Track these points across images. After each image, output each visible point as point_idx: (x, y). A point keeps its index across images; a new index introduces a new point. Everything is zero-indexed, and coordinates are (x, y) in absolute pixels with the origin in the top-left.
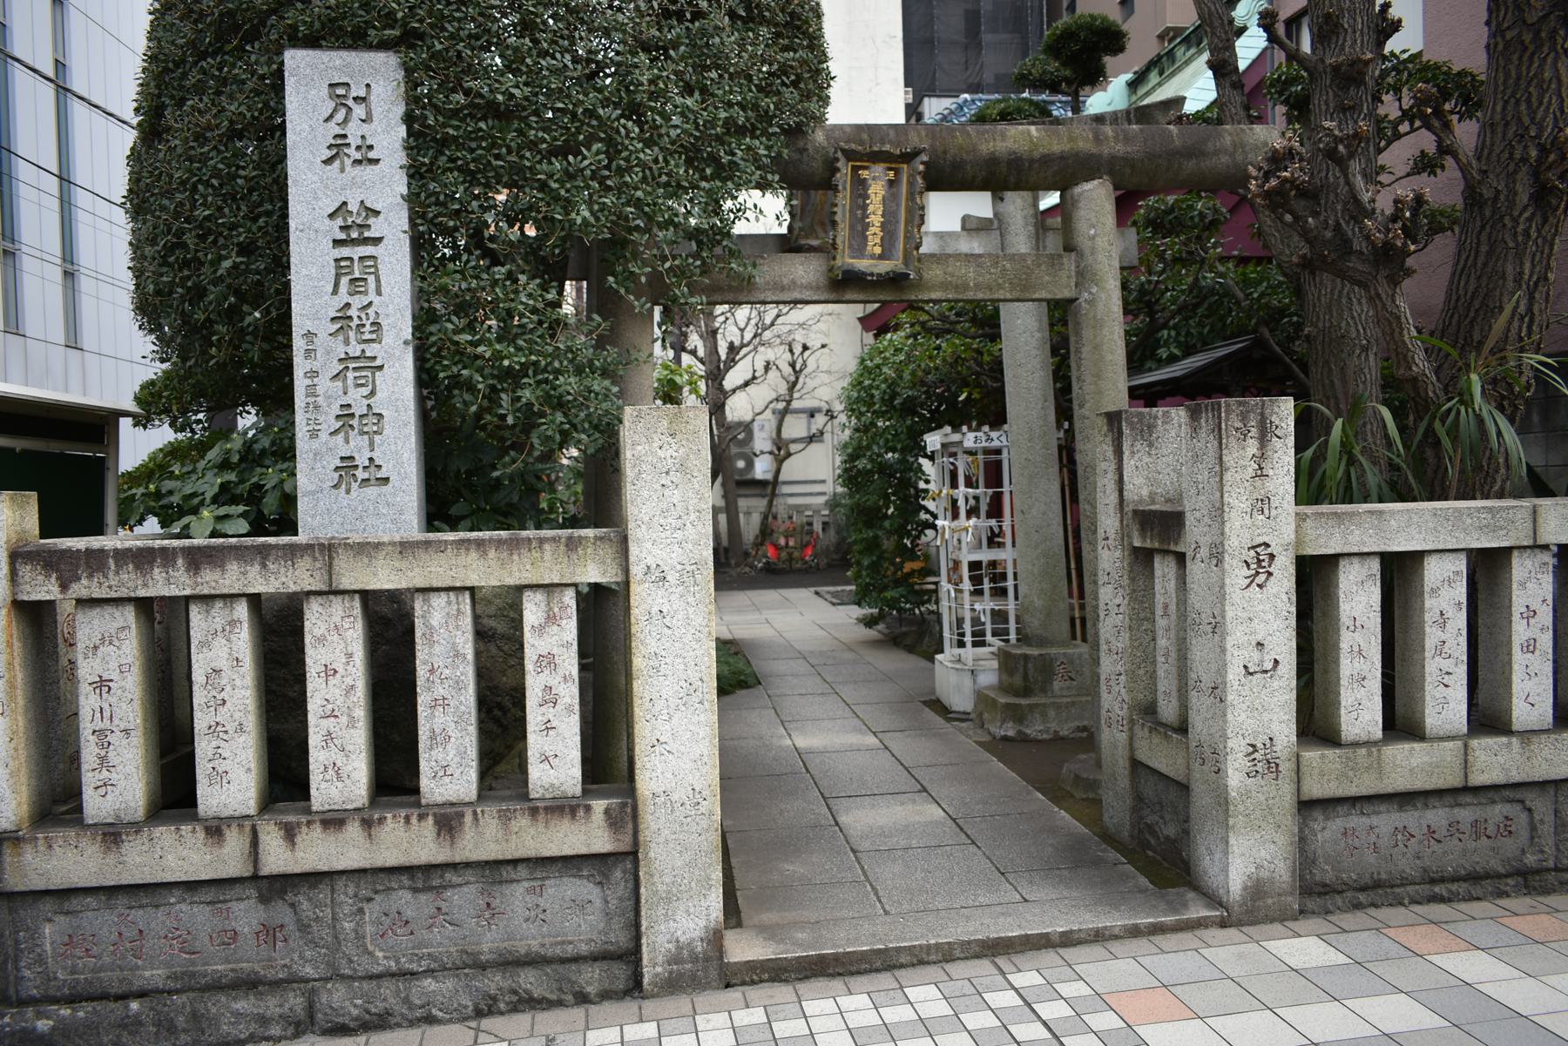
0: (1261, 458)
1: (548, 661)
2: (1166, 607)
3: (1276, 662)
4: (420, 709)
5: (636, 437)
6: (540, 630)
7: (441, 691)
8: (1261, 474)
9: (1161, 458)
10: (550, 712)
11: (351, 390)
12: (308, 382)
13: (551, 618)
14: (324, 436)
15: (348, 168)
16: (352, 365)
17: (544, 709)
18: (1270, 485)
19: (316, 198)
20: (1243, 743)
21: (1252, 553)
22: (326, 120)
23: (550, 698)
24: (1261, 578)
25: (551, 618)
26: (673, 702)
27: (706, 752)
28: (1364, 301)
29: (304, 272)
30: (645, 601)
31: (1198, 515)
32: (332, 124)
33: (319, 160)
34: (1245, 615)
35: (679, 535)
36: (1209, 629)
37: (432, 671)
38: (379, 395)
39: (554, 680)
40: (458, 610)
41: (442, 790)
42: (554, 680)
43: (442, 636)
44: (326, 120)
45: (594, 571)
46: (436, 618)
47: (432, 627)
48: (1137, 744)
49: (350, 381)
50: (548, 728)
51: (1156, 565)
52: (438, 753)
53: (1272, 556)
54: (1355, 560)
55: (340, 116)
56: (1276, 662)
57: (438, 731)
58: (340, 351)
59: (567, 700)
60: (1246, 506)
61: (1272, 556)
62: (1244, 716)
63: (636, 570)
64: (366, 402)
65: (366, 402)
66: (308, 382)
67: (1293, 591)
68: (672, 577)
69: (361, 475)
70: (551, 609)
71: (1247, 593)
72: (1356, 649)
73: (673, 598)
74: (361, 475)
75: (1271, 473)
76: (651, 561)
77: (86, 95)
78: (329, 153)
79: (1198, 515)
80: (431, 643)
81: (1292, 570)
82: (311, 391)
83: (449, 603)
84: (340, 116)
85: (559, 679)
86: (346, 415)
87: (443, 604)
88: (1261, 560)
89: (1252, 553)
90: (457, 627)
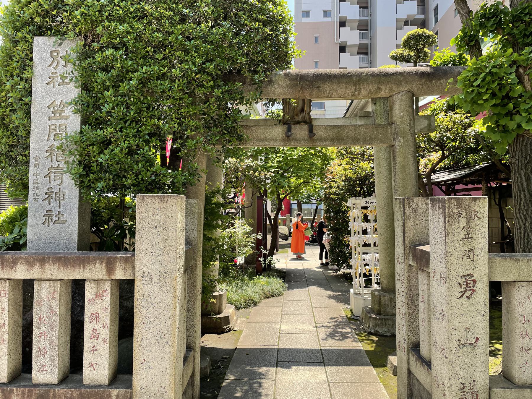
0: (468, 229)
1: (96, 317)
2: (423, 297)
3: (477, 339)
4: (34, 337)
5: (141, 209)
6: (93, 301)
7: (44, 328)
8: (468, 237)
9: (433, 219)
10: (95, 342)
11: (52, 181)
12: (35, 178)
13: (98, 296)
14: (40, 201)
15: (57, 86)
16: (53, 171)
17: (92, 340)
18: (474, 243)
19: (43, 99)
20: (459, 382)
21: (463, 280)
22: (49, 66)
23: (95, 336)
24: (468, 293)
25: (98, 296)
26: (153, 341)
27: (168, 367)
28: (302, 153)
29: (36, 130)
30: (140, 291)
31: (435, 255)
32: (51, 68)
33: (45, 83)
34: (459, 312)
35: (160, 258)
36: (440, 316)
37: (40, 319)
38: (64, 184)
39: (98, 327)
40: (54, 290)
41: (42, 377)
42: (98, 327)
43: (45, 303)
44: (49, 66)
45: (120, 274)
46: (44, 294)
47: (41, 298)
48: (411, 363)
49: (52, 178)
50: (94, 350)
51: (419, 275)
52: (41, 359)
53: (475, 282)
54: (525, 284)
55: (55, 64)
56: (477, 339)
57: (42, 348)
58: (49, 164)
59: (104, 336)
60: (460, 254)
61: (475, 282)
62: (458, 367)
63: (138, 275)
64: (59, 187)
65: (59, 187)
66: (35, 178)
67: (488, 301)
68: (155, 279)
69: (54, 218)
70: (98, 291)
71: (460, 301)
72: (524, 333)
73: (156, 288)
74: (54, 218)
75: (474, 236)
76: (145, 269)
77: (346, 109)
78: (49, 80)
79: (435, 255)
80: (41, 306)
81: (487, 289)
82: (36, 182)
83: (50, 286)
84: (55, 64)
85: (100, 326)
86: (49, 194)
87: (47, 287)
88: (468, 284)
89: (463, 280)
90: (53, 298)
